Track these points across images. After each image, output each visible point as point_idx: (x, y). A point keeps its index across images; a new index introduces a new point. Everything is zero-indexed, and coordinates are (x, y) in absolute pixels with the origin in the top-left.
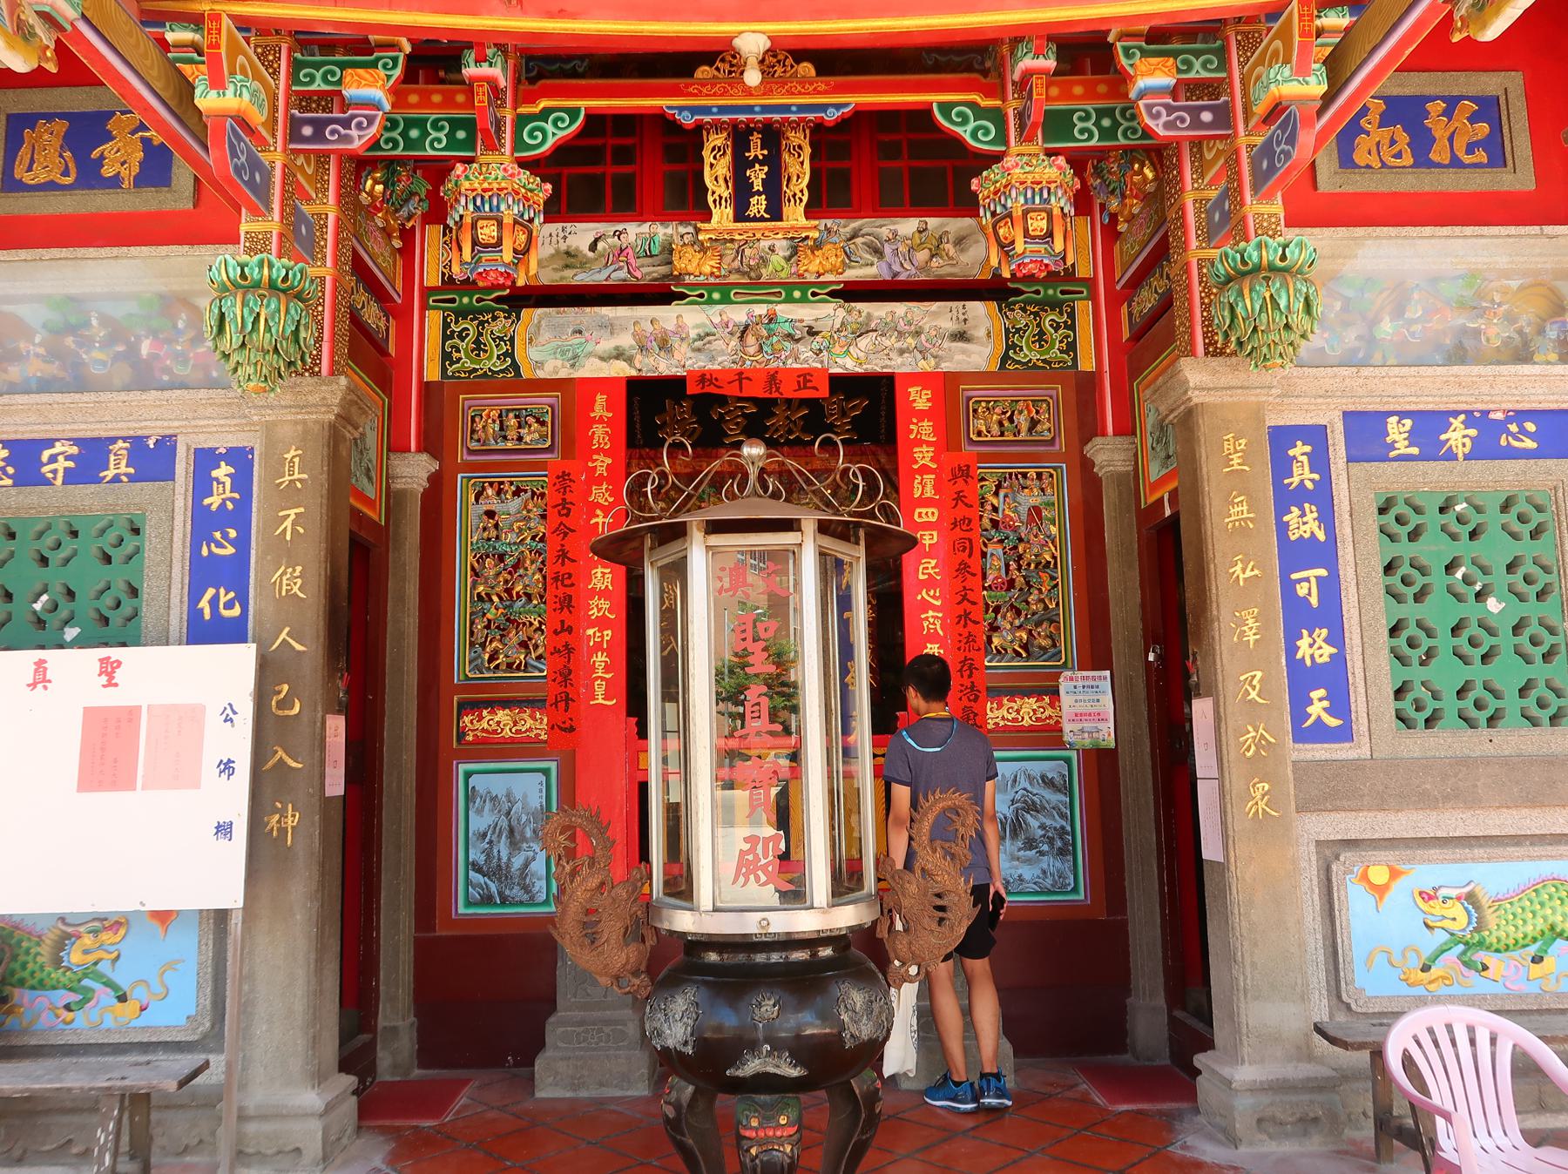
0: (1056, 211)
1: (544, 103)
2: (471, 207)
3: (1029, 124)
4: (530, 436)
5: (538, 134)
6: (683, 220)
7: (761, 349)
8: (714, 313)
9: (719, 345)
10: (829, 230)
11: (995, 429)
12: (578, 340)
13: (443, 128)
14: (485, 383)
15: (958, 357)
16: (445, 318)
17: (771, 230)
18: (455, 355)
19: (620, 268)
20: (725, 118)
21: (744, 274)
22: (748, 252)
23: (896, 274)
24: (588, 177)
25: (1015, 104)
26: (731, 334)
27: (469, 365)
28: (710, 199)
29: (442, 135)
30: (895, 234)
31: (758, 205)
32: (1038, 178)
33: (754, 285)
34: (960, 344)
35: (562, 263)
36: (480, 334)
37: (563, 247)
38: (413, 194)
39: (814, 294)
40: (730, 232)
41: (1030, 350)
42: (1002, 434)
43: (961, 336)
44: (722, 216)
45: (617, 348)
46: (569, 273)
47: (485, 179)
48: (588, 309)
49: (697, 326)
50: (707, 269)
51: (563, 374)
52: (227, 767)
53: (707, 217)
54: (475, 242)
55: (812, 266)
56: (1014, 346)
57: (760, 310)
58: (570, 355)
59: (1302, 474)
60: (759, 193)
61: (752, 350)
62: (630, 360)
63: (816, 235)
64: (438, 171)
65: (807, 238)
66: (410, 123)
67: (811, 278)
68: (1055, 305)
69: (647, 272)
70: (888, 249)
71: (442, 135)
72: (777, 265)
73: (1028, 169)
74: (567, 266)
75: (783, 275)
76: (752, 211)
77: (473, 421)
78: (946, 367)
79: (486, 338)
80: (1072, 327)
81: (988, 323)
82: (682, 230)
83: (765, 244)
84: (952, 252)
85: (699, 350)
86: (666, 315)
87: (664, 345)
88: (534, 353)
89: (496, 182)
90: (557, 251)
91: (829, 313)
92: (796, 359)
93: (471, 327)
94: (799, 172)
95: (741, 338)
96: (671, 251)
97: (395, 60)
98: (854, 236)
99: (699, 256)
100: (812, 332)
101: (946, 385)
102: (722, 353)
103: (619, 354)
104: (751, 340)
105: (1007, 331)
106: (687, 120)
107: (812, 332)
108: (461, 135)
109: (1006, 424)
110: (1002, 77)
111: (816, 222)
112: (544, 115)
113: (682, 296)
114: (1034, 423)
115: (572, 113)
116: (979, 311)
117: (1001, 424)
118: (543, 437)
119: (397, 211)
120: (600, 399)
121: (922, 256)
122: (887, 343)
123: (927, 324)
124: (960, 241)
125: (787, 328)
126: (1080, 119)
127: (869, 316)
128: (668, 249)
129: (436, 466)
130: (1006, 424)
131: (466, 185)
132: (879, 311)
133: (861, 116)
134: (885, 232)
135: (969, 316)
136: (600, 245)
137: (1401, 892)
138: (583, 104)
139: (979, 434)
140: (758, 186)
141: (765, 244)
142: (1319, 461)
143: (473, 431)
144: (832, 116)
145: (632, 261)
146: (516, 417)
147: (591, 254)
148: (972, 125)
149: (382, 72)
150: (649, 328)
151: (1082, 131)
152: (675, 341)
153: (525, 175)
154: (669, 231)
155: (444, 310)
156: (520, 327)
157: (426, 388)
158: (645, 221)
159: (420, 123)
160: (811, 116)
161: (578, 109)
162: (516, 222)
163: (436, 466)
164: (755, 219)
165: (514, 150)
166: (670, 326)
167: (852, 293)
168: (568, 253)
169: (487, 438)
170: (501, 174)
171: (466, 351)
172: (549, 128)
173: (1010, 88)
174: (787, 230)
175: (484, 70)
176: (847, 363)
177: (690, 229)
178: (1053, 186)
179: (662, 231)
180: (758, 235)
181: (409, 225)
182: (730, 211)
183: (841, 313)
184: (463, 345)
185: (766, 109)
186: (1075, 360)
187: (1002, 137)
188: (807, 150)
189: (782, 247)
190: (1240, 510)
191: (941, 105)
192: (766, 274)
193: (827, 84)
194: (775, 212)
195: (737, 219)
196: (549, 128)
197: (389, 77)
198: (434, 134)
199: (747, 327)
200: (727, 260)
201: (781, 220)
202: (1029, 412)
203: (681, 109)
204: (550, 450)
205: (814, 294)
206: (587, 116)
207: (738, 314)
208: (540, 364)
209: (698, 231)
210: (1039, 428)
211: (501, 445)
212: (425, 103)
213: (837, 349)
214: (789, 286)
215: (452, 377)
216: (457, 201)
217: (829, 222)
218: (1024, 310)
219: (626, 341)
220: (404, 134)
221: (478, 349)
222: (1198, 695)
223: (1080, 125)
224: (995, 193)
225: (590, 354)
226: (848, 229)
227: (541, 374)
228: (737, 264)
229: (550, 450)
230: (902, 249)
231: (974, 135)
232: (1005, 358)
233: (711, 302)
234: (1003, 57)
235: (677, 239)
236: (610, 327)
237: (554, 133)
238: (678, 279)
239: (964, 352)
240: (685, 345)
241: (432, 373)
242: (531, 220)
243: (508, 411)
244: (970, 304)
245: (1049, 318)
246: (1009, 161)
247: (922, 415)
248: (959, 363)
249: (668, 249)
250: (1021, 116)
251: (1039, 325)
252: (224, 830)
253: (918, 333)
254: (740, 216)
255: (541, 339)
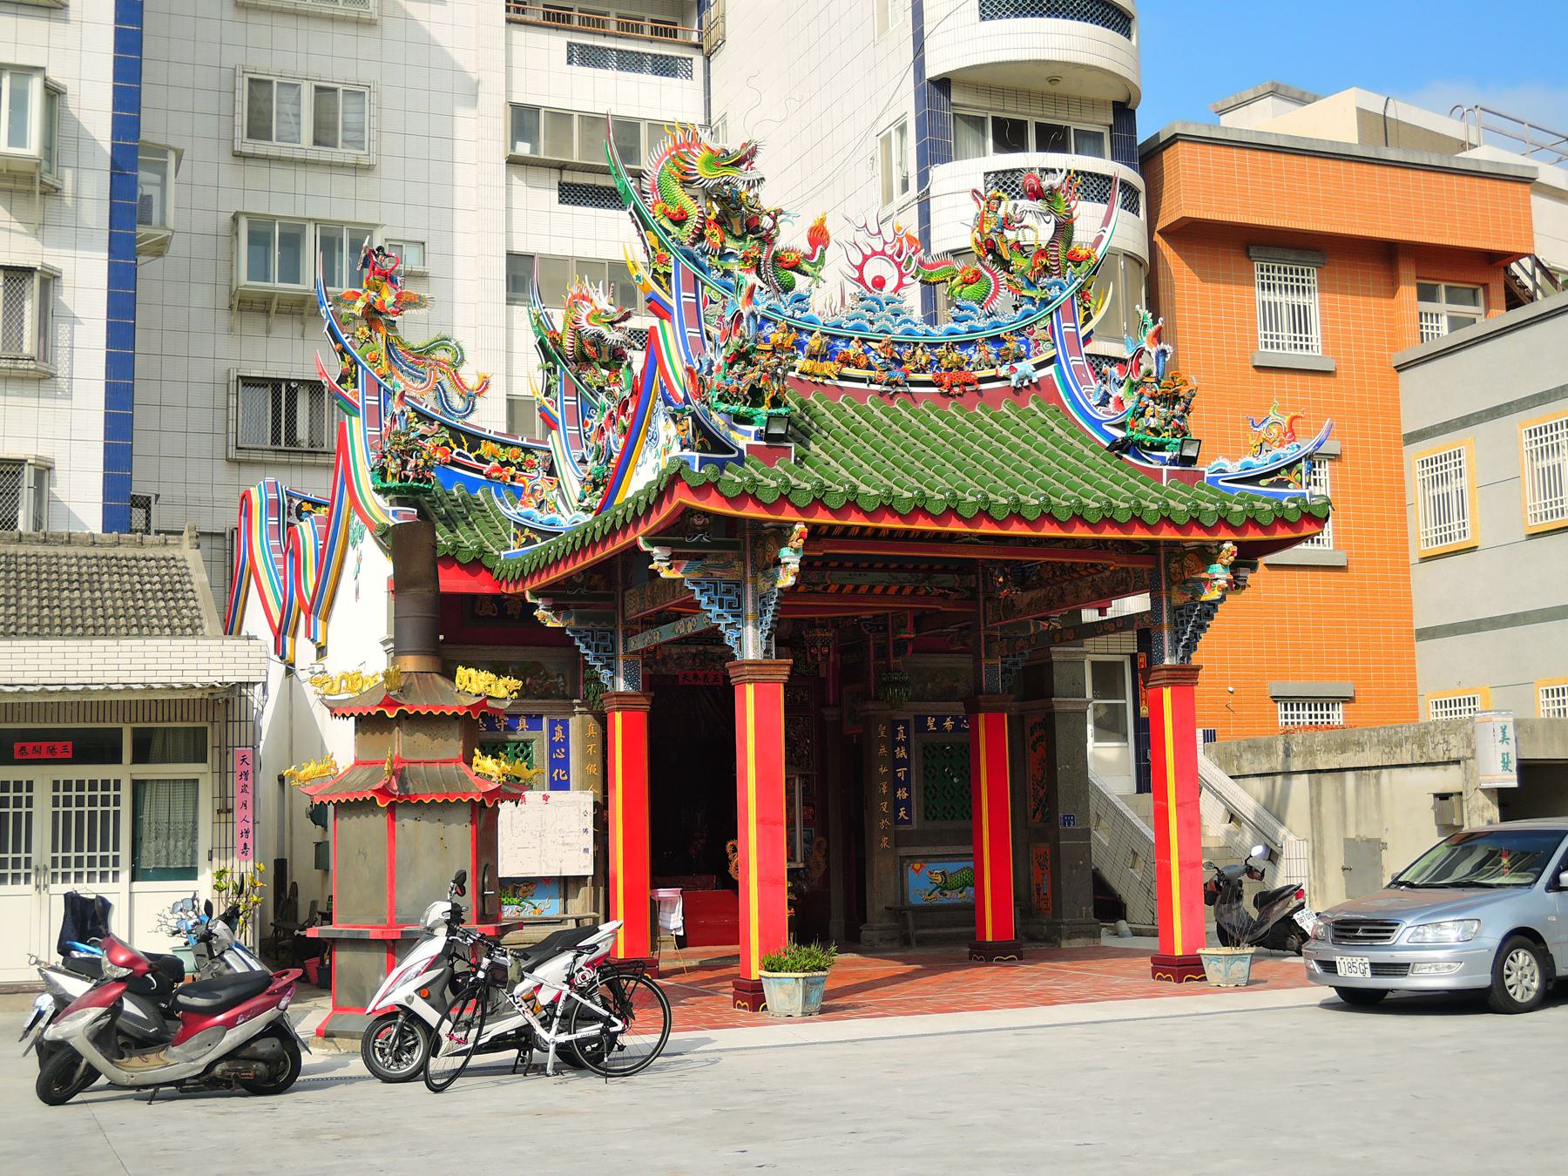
52: (586, 831)
59: (901, 737)
137: (925, 872)
142: (906, 732)
190: (883, 750)
222: (531, 788)
252: (586, 850)
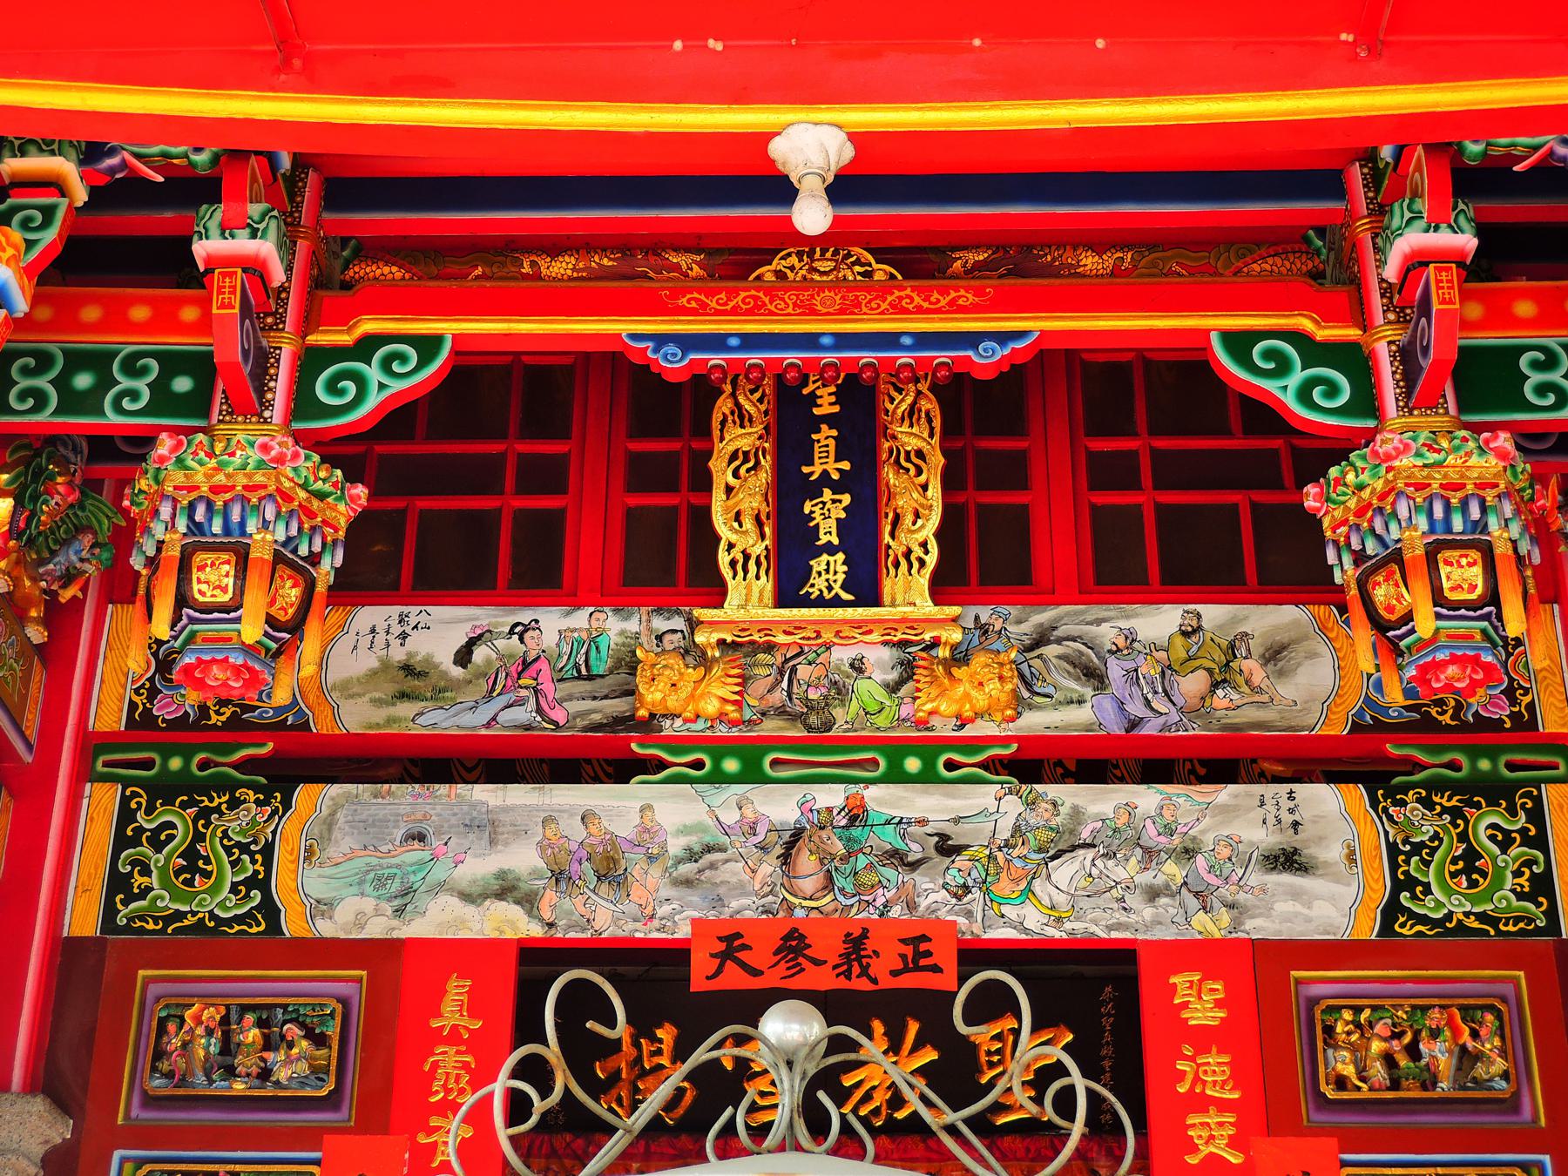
0: (1502, 549)
1: (370, 325)
2: (182, 524)
3: (1426, 363)
4: (291, 1067)
5: (351, 387)
6: (662, 607)
7: (829, 884)
8: (727, 803)
9: (734, 871)
10: (984, 629)
11: (1378, 1071)
12: (415, 854)
13: (144, 371)
14: (204, 942)
15: (1283, 907)
16: (125, 801)
17: (856, 624)
18: (139, 880)
19: (520, 702)
20: (755, 358)
21: (795, 718)
22: (804, 672)
23: (1134, 723)
24: (465, 494)
25: (1390, 332)
26: (763, 848)
27: (167, 904)
28: (723, 559)
29: (141, 385)
30: (1131, 637)
31: (828, 572)
32: (1454, 477)
33: (817, 744)
34: (1287, 878)
35: (392, 688)
36: (199, 837)
37: (398, 654)
38: (80, 529)
39: (951, 765)
40: (765, 627)
41: (1449, 892)
42: (1395, 1085)
43: (1288, 860)
44: (748, 599)
45: (501, 875)
46: (406, 709)
47: (217, 469)
48: (442, 789)
49: (685, 830)
50: (711, 707)
51: (377, 929)
53: (717, 595)
54: (183, 600)
55: (942, 705)
56: (1410, 883)
57: (831, 797)
58: (395, 887)
60: (830, 549)
61: (809, 885)
62: (529, 902)
63: (957, 636)
64: (124, 452)
65: (936, 643)
66: (76, 360)
67: (944, 728)
68: (1496, 792)
69: (578, 710)
70: (1115, 670)
71: (141, 385)
72: (870, 702)
73: (1432, 457)
74: (403, 696)
75: (881, 721)
76: (817, 586)
77: (162, 1029)
78: (1258, 927)
79: (212, 847)
80: (1540, 842)
81: (1345, 832)
82: (660, 624)
83: (842, 655)
84: (1259, 676)
85: (687, 883)
86: (618, 806)
87: (611, 871)
88: (316, 883)
89: (247, 478)
90: (385, 665)
91: (987, 808)
92: (911, 906)
93: (180, 820)
94: (918, 515)
95: (786, 858)
96: (632, 666)
97: (48, 213)
98: (1041, 639)
99: (693, 674)
100: (947, 848)
101: (1261, 967)
102: (741, 889)
103: (506, 889)
104: (806, 861)
105: (1393, 849)
106: (672, 362)
107: (947, 848)
108: (182, 384)
109: (1403, 1061)
110: (1357, 284)
111: (955, 610)
112: (365, 348)
113: (654, 766)
114: (1467, 1059)
115: (427, 346)
116: (1325, 804)
117: (1389, 1060)
118: (318, 1072)
119: (42, 562)
120: (456, 991)
121: (1192, 684)
122: (1120, 873)
123: (1208, 832)
124: (1274, 654)
125: (889, 838)
126: (1536, 365)
127: (1077, 814)
128: (628, 663)
129: (60, 1131)
130: (1403, 1061)
131: (179, 478)
132: (1100, 803)
133: (1053, 358)
134: (1107, 634)
135: (1304, 815)
136: (480, 654)
138: (448, 328)
139: (1341, 1083)
140: (828, 533)
141: (842, 655)
143: (159, 1054)
144: (988, 356)
145: (547, 687)
146: (261, 1024)
147: (457, 672)
148: (1297, 376)
149: (16, 235)
150: (577, 832)
151: (1541, 390)
152: (634, 863)
153: (307, 462)
154: (633, 625)
155: (126, 782)
156: (290, 825)
157: (66, 952)
158: (578, 605)
159: (99, 362)
160: (942, 356)
161: (435, 341)
162: (278, 558)
163: (60, 1131)
164: (820, 602)
165: (293, 413)
166: (625, 829)
167: (1030, 764)
168: (408, 669)
169: (190, 1071)
170: (255, 455)
171: (163, 871)
172: (373, 373)
173: (1377, 302)
174: (889, 625)
175: (242, 244)
176: (1026, 919)
177: (678, 623)
178: (1490, 496)
179: (617, 627)
180: (827, 636)
181: (66, 595)
182: (766, 585)
183: (1013, 806)
184: (157, 860)
185: (844, 341)
186: (1552, 914)
187: (1367, 401)
188: (938, 460)
189: (881, 659)
191: (1229, 337)
192: (843, 718)
193: (979, 292)
194: (865, 588)
195: (782, 600)
196: (373, 373)
197: (30, 244)
198: (125, 383)
199: (798, 834)
200: (759, 687)
201: (876, 601)
202: (1456, 1033)
203: (661, 340)
204: (331, 1102)
205: (951, 765)
206: (454, 352)
207: (780, 806)
208: (324, 907)
209: (693, 624)
210: (1480, 1070)
211: (220, 1087)
212: (116, 321)
213: (1004, 886)
214: (896, 748)
215: (127, 929)
216: (155, 513)
217: (985, 613)
218: (1428, 804)
219: (524, 859)
220: (62, 383)
221: (192, 868)
223: (1536, 377)
224: (1360, 513)
225: (440, 887)
226: (1026, 627)
227: (326, 929)
228: (779, 696)
229: (331, 1102)
230: (1149, 670)
231: (1304, 395)
232: (1392, 910)
233: (719, 778)
234: (1356, 245)
235: (648, 641)
236: (490, 829)
237: (383, 385)
238: (648, 726)
239: (1296, 895)
240: (655, 871)
241: (82, 918)
242: (314, 559)
243: (245, 1009)
244: (1303, 790)
245: (1485, 821)
246: (1387, 442)
247: (1204, 1039)
248: (1287, 919)
249: (628, 663)
250: (1406, 356)
251: (1463, 837)
253: (1188, 853)
254: (789, 592)
255: (333, 852)
